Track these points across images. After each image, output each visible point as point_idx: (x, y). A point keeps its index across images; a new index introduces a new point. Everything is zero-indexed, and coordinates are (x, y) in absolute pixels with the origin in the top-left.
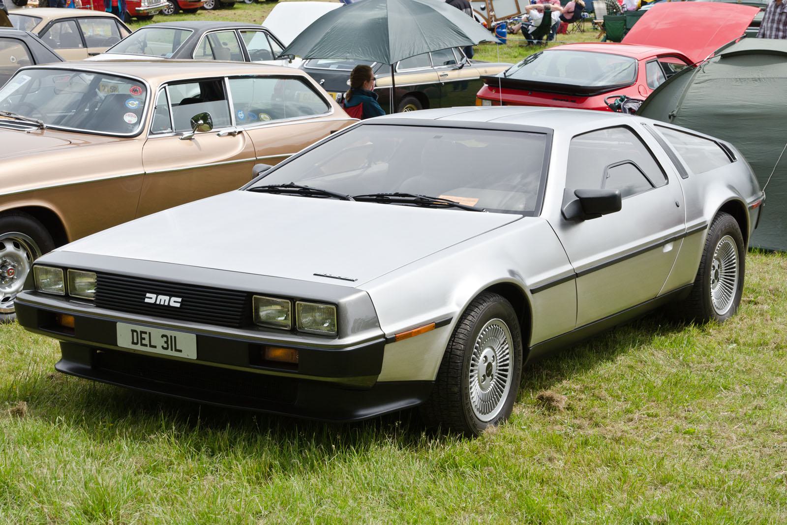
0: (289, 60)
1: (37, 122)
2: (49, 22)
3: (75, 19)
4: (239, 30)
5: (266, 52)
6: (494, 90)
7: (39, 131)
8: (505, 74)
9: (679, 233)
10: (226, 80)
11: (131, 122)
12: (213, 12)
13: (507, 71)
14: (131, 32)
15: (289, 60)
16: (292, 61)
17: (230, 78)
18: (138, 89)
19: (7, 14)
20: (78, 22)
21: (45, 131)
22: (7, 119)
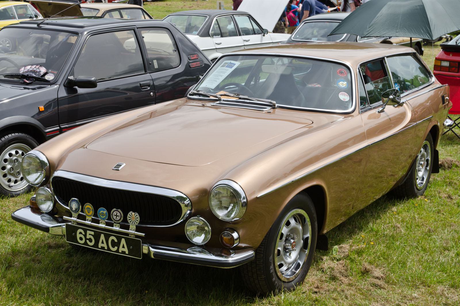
0: (263, 34)
1: (271, 103)
2: (104, 13)
3: (119, 10)
4: (234, 15)
5: (247, 29)
6: (451, 54)
7: (272, 111)
8: (456, 42)
9: (409, 126)
10: (385, 58)
11: (345, 100)
12: (152, 2)
13: (458, 40)
14: (123, 18)
15: (263, 34)
16: (265, 35)
17: (387, 57)
18: (343, 71)
19: (80, 7)
20: (120, 12)
21: (277, 110)
22: (234, 99)
